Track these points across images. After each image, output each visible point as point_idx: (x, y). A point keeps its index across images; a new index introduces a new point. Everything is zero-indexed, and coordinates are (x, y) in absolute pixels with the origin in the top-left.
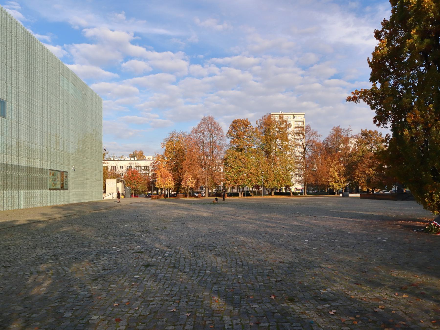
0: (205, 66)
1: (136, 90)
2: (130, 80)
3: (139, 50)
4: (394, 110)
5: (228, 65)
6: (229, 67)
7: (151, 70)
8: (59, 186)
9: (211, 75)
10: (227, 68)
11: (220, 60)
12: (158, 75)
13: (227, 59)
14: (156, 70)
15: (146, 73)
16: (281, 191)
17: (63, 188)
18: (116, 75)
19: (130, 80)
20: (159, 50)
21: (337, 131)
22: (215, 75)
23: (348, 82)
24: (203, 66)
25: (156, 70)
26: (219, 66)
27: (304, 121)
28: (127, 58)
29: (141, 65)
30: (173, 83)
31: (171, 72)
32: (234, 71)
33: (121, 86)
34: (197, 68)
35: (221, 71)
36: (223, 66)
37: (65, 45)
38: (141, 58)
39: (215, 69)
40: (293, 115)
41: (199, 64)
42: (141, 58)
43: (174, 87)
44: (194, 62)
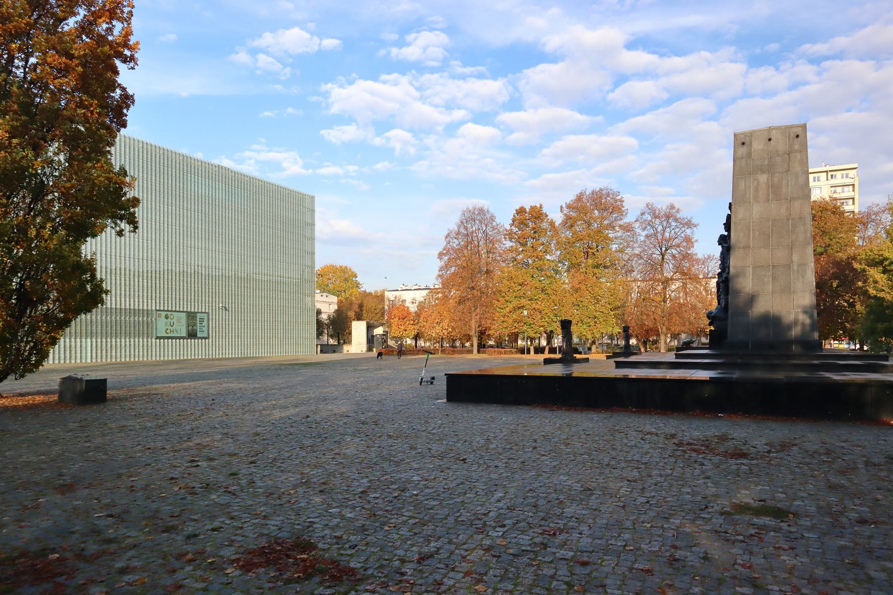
0: (782, 68)
1: (632, 141)
2: (621, 125)
3: (641, 58)
4: (96, 155)
5: (840, 56)
6: (842, 60)
7: (665, 96)
8: (184, 333)
9: (793, 87)
10: (838, 63)
11: (821, 48)
12: (678, 106)
13: (841, 42)
14: (676, 96)
15: (654, 106)
16: (578, 371)
17: (192, 335)
18: (600, 118)
19: (621, 125)
20: (679, 52)
21: (672, 207)
22: (805, 83)
23: (861, 60)
24: (777, 69)
25: (676, 96)
26: (815, 60)
27: (856, 184)
28: (621, 79)
29: (644, 89)
30: (713, 118)
31: (706, 94)
32: (854, 66)
33: (605, 139)
34: (765, 73)
35: (819, 74)
36: (827, 58)
37: (510, 76)
38: (646, 74)
39: (807, 71)
40: (827, 172)
41: (769, 65)
42: (646, 74)
43: (713, 126)
44: (756, 62)
